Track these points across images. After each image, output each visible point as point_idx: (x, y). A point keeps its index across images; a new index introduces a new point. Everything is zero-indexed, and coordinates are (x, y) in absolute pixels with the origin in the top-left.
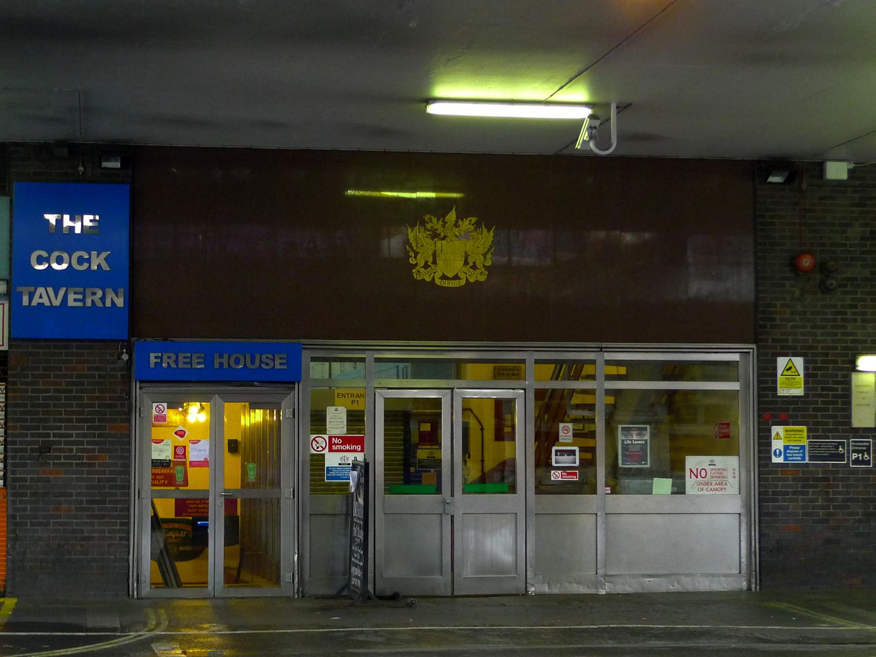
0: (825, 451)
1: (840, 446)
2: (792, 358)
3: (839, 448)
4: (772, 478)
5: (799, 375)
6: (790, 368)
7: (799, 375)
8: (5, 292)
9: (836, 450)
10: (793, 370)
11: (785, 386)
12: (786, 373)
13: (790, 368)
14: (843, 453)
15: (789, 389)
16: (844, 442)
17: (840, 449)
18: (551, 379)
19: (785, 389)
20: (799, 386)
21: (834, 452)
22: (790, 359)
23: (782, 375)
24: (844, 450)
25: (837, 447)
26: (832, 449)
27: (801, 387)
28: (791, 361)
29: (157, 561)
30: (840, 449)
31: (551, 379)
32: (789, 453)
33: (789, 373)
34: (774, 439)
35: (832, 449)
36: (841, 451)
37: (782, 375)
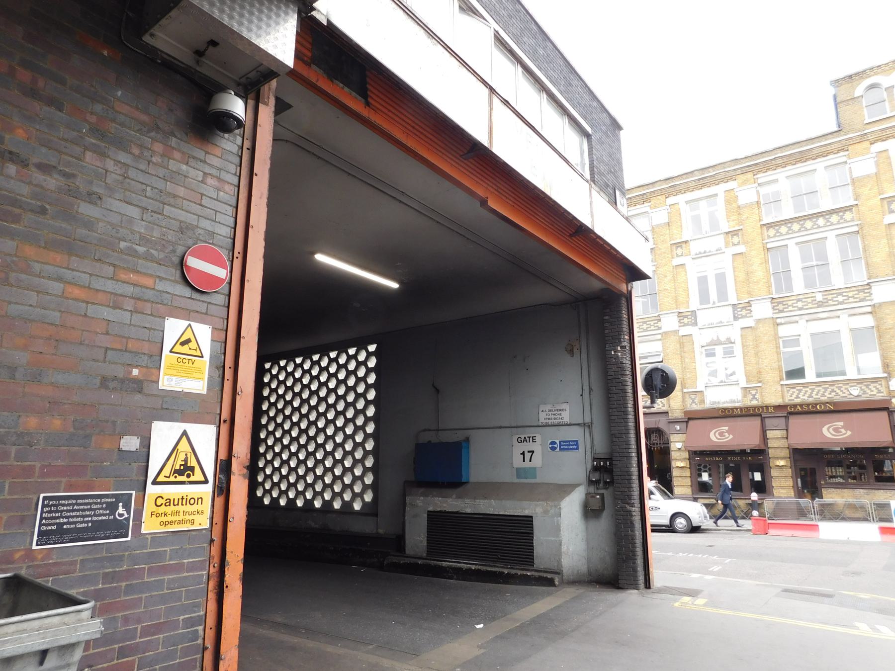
0: (83, 516)
1: (121, 504)
2: (192, 324)
3: (117, 509)
4: (170, 581)
5: (202, 357)
6: (188, 341)
7: (202, 357)
8: (694, 525)
9: (109, 515)
10: (193, 345)
11: (174, 372)
12: (178, 348)
13: (188, 341)
14: (125, 519)
15: (183, 379)
16: (131, 494)
17: (121, 510)
18: (279, 75)
19: (174, 378)
20: (199, 375)
21: (104, 518)
22: (190, 325)
23: (171, 352)
24: (129, 513)
25: (113, 508)
26: (101, 512)
27: (641, 358)
28: (191, 327)
29: (186, 266)
30: (121, 510)
31: (279, 75)
32: (563, 445)
33: (185, 349)
34: (155, 482)
35: (101, 512)
36: (121, 515)
37: (171, 352)
